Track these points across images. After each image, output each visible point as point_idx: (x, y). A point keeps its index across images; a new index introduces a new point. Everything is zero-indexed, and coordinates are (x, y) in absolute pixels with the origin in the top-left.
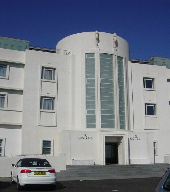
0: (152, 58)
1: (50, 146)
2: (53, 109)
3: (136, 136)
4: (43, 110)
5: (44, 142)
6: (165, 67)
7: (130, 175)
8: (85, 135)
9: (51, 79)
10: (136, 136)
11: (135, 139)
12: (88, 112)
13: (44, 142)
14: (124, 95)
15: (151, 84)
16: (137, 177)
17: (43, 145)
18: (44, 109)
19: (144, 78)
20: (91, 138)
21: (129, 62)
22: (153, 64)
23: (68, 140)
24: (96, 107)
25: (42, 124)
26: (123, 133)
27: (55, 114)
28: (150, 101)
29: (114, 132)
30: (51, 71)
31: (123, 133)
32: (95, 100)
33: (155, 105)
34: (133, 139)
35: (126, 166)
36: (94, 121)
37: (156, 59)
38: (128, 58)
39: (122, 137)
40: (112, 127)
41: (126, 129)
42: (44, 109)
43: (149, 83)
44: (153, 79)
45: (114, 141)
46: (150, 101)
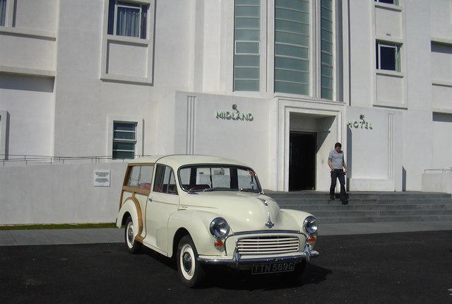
1: (132, 136)
2: (144, 36)
3: (362, 117)
4: (114, 37)
5: (117, 125)
8: (234, 107)
9: (132, 33)
10: (362, 117)
11: (360, 125)
12: (238, 47)
13: (117, 125)
14: (332, 79)
17: (115, 135)
18: (118, 34)
19: (378, 42)
20: (251, 117)
23: (187, 131)
24: (262, 35)
25: (114, 74)
27: (148, 50)
28: (387, 34)
29: (311, 104)
30: (133, 10)
32: (258, 65)
33: (399, 45)
34: (356, 125)
36: (256, 73)
40: (302, 90)
41: (335, 99)
42: (118, 34)
45: (308, 128)
46: (387, 34)
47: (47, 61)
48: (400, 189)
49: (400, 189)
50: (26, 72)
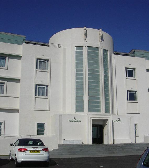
0: (133, 50)
1: (44, 127)
2: (46, 96)
3: (119, 119)
4: (37, 96)
5: (38, 124)
6: (144, 59)
7: (114, 153)
8: (75, 118)
9: (44, 69)
10: (119, 119)
11: (118, 121)
12: (77, 98)
13: (38, 124)
15: (133, 73)
16: (120, 155)
17: (38, 127)
18: (38, 95)
20: (80, 121)
21: (113, 55)
22: (134, 56)
24: (84, 94)
25: (37, 108)
26: (108, 117)
27: (48, 100)
28: (131, 88)
29: (100, 116)
30: (44, 62)
31: (108, 117)
33: (136, 92)
34: (117, 121)
35: (111, 145)
36: (83, 106)
37: (137, 52)
38: (112, 51)
39: (107, 120)
40: (98, 111)
41: (111, 113)
42: (38, 95)
43: (130, 73)
44: (134, 69)
45: (100, 123)
46: (131, 88)
47: (17, 106)
48: (134, 142)
49: (134, 142)
50: (10, 109)
